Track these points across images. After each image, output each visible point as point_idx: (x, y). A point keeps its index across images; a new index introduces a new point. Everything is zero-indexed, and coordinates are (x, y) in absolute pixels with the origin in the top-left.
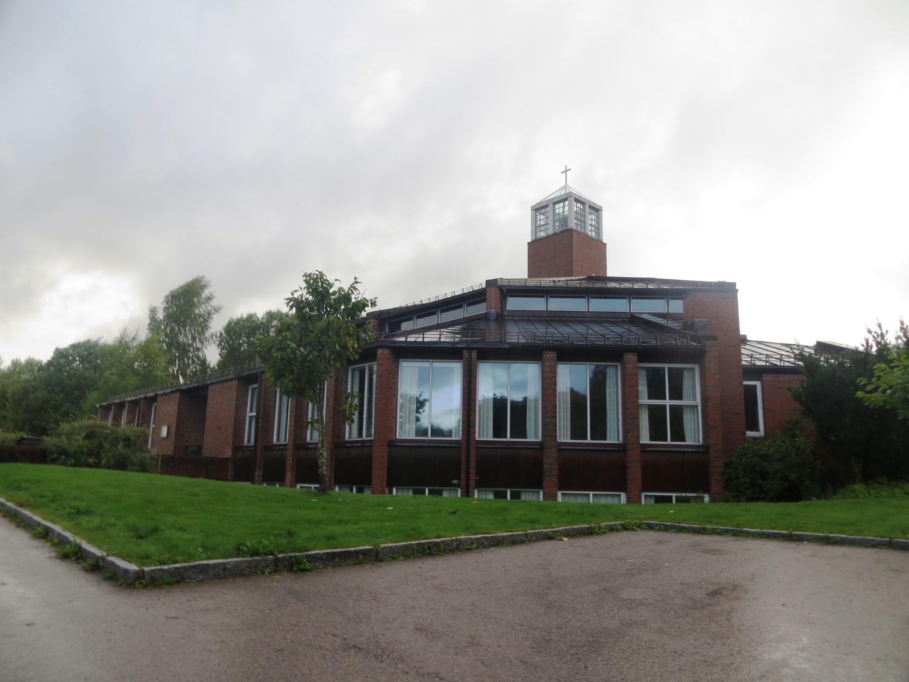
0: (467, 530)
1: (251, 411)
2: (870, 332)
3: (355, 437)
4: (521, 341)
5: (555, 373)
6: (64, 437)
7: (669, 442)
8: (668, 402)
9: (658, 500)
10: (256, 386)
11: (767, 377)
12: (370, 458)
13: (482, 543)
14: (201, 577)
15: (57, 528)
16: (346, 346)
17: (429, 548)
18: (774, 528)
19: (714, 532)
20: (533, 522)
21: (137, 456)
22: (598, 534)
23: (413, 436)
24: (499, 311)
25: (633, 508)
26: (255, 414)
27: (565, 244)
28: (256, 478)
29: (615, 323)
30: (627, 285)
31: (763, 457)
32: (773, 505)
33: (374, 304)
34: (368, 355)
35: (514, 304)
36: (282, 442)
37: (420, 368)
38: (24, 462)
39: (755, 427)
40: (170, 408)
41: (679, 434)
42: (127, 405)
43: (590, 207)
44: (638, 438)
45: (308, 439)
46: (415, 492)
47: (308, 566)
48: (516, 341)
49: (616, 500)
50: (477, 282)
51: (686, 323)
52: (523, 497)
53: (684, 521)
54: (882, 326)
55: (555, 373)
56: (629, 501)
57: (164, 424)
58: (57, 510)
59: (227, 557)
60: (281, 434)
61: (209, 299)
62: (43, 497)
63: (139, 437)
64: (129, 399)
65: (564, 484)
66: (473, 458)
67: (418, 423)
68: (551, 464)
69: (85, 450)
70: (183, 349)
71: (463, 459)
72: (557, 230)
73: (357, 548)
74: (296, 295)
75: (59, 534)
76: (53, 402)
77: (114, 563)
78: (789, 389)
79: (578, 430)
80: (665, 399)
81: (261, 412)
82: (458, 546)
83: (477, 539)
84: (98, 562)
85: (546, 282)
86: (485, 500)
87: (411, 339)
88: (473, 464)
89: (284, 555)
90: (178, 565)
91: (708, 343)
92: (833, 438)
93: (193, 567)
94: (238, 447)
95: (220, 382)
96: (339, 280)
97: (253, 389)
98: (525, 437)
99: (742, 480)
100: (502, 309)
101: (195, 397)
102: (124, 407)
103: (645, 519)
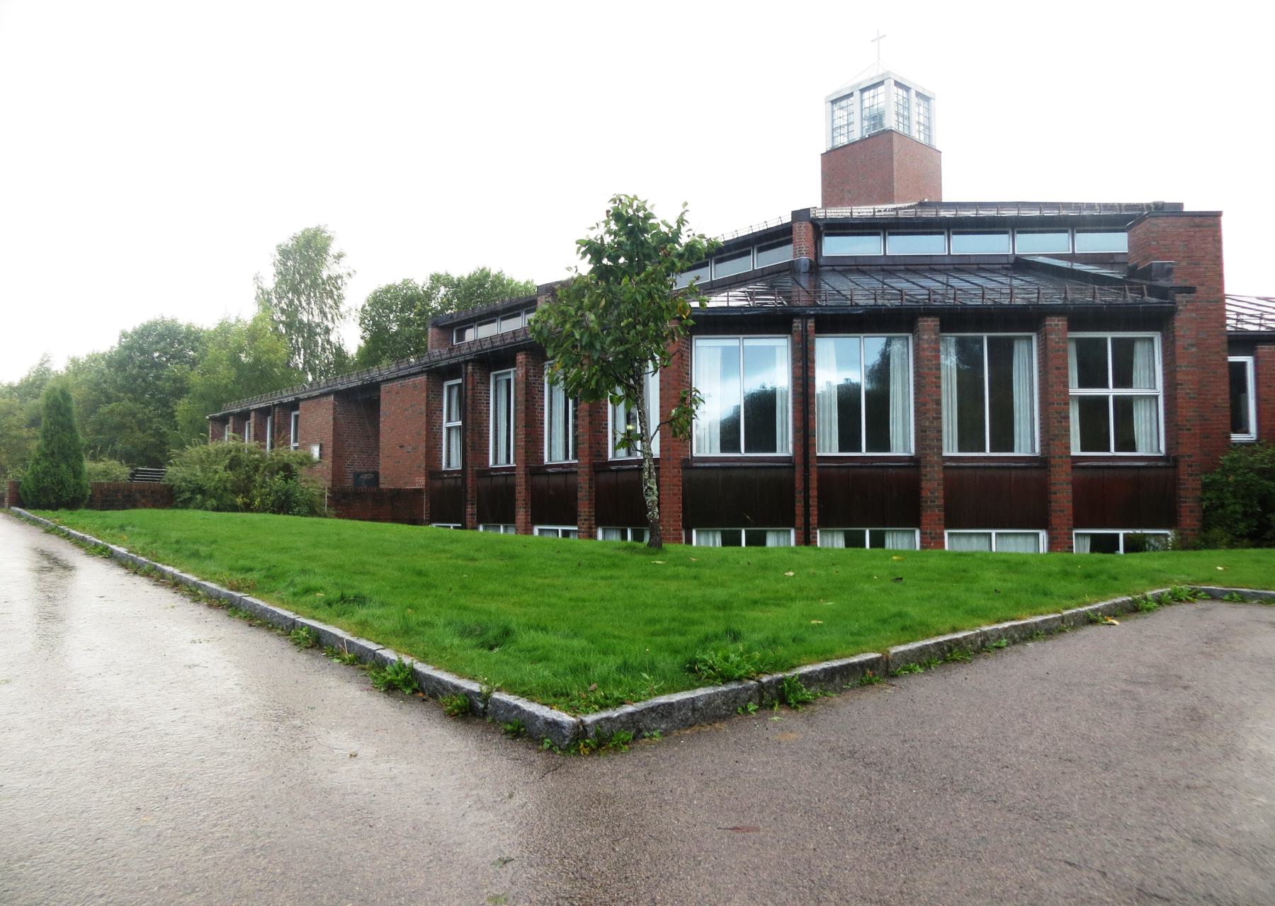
8: (1111, 392)
11: (1264, 349)
23: (717, 453)
27: (863, 162)
28: (469, 517)
30: (971, 213)
35: (834, 247)
36: (502, 463)
37: (724, 348)
38: (145, 506)
40: (320, 418)
41: (1127, 441)
42: (253, 414)
43: (918, 94)
49: (984, 541)
50: (778, 216)
56: (1052, 546)
57: (314, 442)
61: (339, 257)
64: (256, 407)
65: (953, 520)
66: (814, 484)
70: (309, 331)
71: (799, 484)
79: (848, 438)
82: (983, 643)
83: (1005, 630)
88: (814, 493)
93: (652, 710)
94: (433, 473)
97: (450, 388)
98: (888, 449)
102: (248, 418)
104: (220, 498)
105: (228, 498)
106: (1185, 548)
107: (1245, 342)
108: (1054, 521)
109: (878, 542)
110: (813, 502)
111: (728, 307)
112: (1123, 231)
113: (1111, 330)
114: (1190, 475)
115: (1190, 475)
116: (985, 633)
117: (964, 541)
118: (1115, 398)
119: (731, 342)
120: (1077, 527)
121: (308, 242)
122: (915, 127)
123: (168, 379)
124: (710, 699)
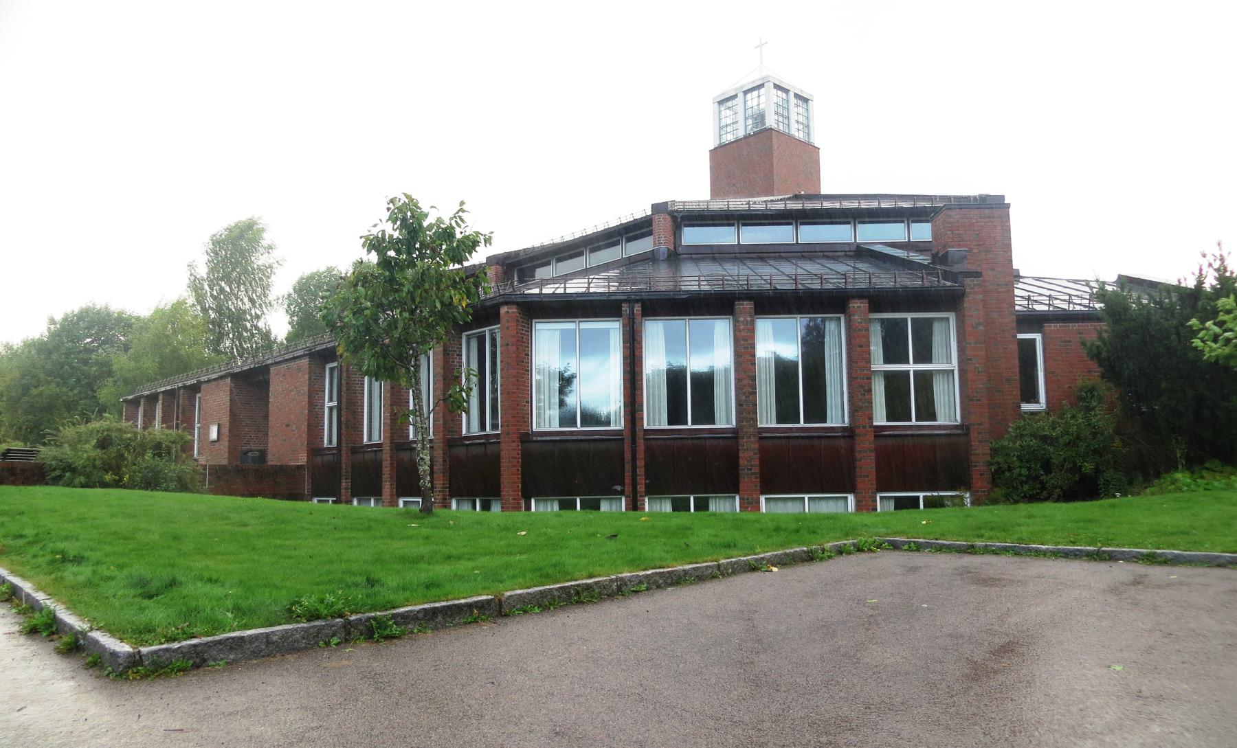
0: (634, 563)
1: (331, 400)
2: (1204, 256)
3: (475, 429)
4: (703, 288)
5: (752, 331)
6: (66, 447)
8: (911, 367)
9: (901, 504)
10: (335, 364)
11: (1051, 327)
12: (497, 458)
13: (656, 582)
14: (232, 657)
15: (26, 586)
16: (451, 304)
17: (578, 593)
18: (1074, 543)
19: (987, 551)
20: (728, 546)
21: (172, 469)
22: (821, 559)
23: (555, 427)
25: (866, 518)
27: (759, 157)
28: (343, 491)
29: (834, 259)
31: (1044, 439)
32: (1063, 506)
33: (488, 241)
34: (486, 314)
35: (693, 236)
37: (562, 330)
38: (14, 483)
39: (1033, 398)
41: (927, 411)
42: (161, 397)
43: (797, 96)
44: (871, 419)
45: (464, 431)
47: (395, 630)
48: (696, 288)
49: (841, 503)
50: (639, 209)
51: (937, 254)
52: (713, 507)
53: (943, 536)
54: (1223, 245)
55: (753, 331)
56: (859, 507)
57: (213, 423)
58: (35, 556)
59: (271, 625)
60: (373, 430)
62: (21, 536)
63: (173, 442)
65: (769, 485)
66: (641, 455)
67: (564, 409)
69: (98, 463)
70: (238, 318)
71: (628, 456)
72: (750, 131)
73: (469, 600)
74: (375, 231)
75: (28, 595)
77: (97, 642)
79: (786, 411)
82: (619, 588)
84: (77, 640)
85: (738, 203)
86: (660, 514)
87: (548, 290)
88: (641, 463)
89: (359, 616)
90: (194, 641)
91: (968, 281)
92: (1144, 409)
93: (220, 642)
96: (437, 210)
97: (332, 369)
101: (252, 383)
103: (888, 535)
104: (88, 476)
105: (95, 477)
106: (979, 505)
107: (1032, 320)
108: (860, 485)
109: (702, 506)
110: (641, 471)
111: (588, 294)
112: (927, 221)
113: (909, 311)
114: (980, 442)
115: (980, 442)
116: (622, 579)
117: (780, 504)
119: (569, 325)
120: (882, 491)
121: (241, 236)
122: (794, 126)
123: (97, 363)
124: (285, 635)
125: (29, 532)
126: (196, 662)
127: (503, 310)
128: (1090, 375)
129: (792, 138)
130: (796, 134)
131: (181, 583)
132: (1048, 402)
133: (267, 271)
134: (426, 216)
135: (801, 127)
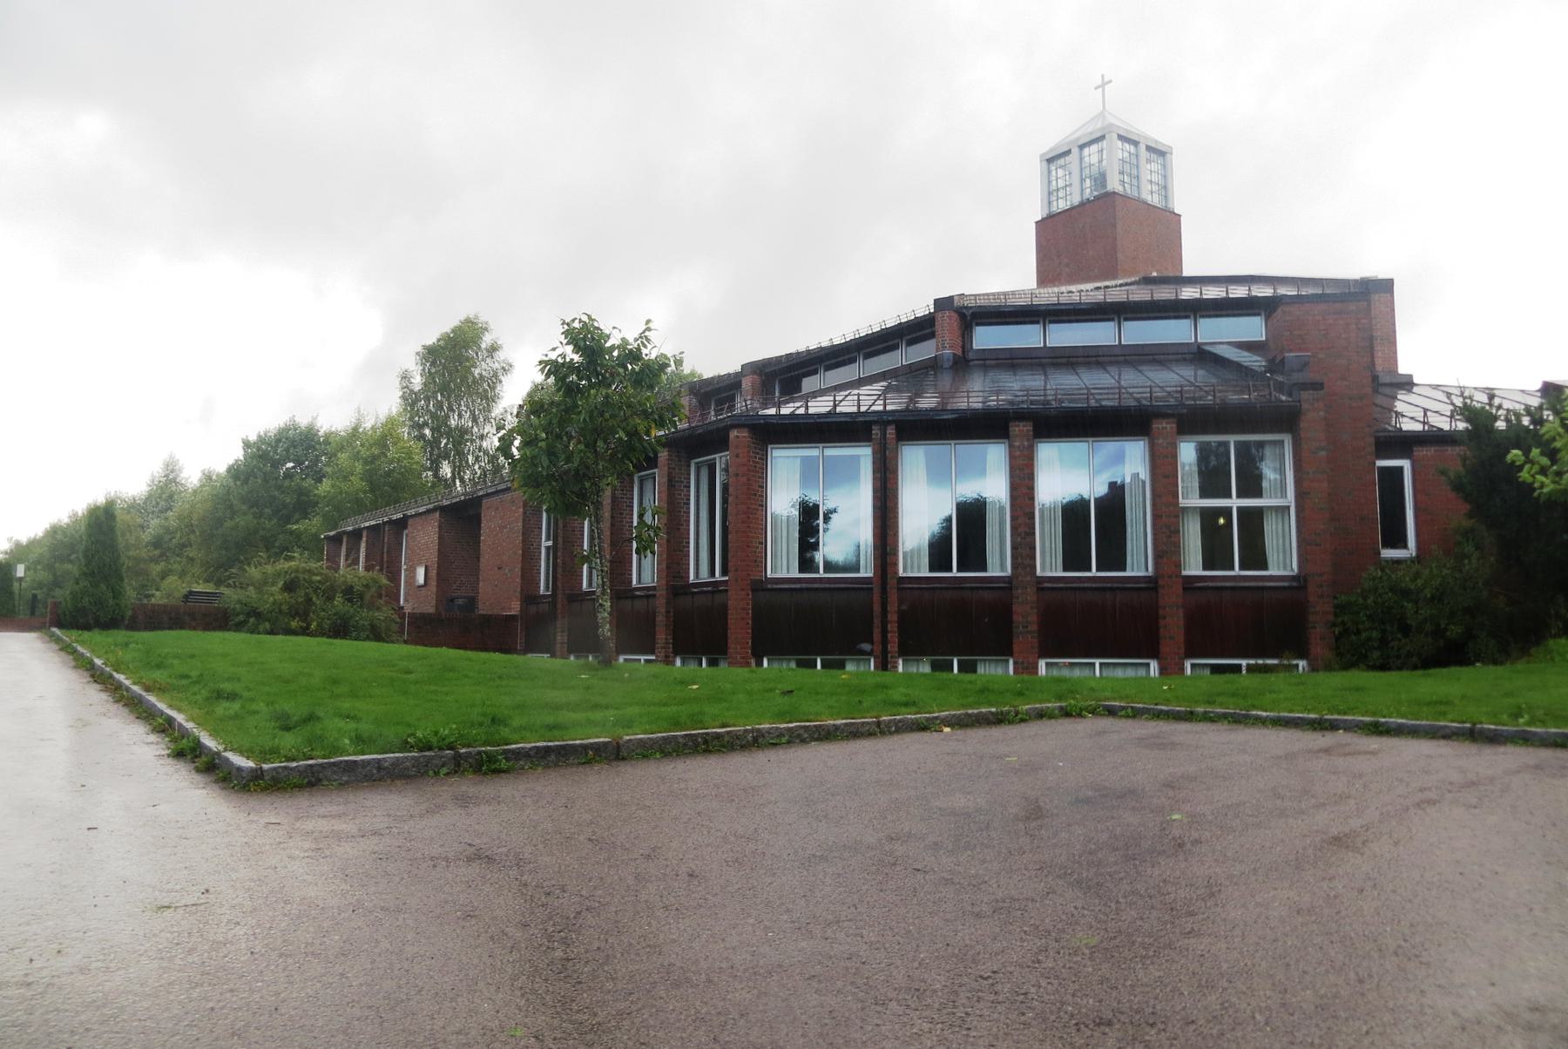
0: (781, 716)
1: (548, 539)
7: (1237, 571)
11: (1420, 452)
12: (724, 610)
13: (799, 736)
15: (180, 718)
17: (706, 742)
21: (364, 616)
24: (959, 353)
26: (550, 543)
27: (1101, 229)
31: (1406, 594)
34: (713, 440)
35: (987, 338)
37: (804, 459)
38: (194, 628)
39: (1401, 542)
40: (424, 539)
41: (1255, 555)
43: (1149, 148)
44: (1178, 566)
46: (936, 667)
47: (504, 764)
49: (1142, 672)
50: (922, 306)
51: (1274, 359)
52: (981, 669)
57: (420, 564)
63: (367, 586)
66: (893, 607)
68: (1026, 615)
71: (877, 608)
74: (553, 356)
76: (262, 533)
78: (1443, 473)
79: (1074, 555)
80: (1230, 496)
81: (560, 540)
82: (755, 740)
85: (1082, 292)
91: (1305, 395)
93: (334, 764)
95: (497, 492)
96: (620, 329)
98: (984, 569)
99: (1364, 635)
100: (963, 347)
101: (463, 518)
102: (360, 538)
107: (1404, 443)
108: (1165, 648)
110: (893, 627)
118: (1239, 509)
119: (812, 452)
125: (194, 674)
126: (310, 781)
127: (733, 434)
128: (1457, 514)
129: (1145, 203)
130: (1149, 198)
131: (319, 718)
132: (1418, 548)
133: (494, 379)
134: (608, 337)
135: (1155, 188)
